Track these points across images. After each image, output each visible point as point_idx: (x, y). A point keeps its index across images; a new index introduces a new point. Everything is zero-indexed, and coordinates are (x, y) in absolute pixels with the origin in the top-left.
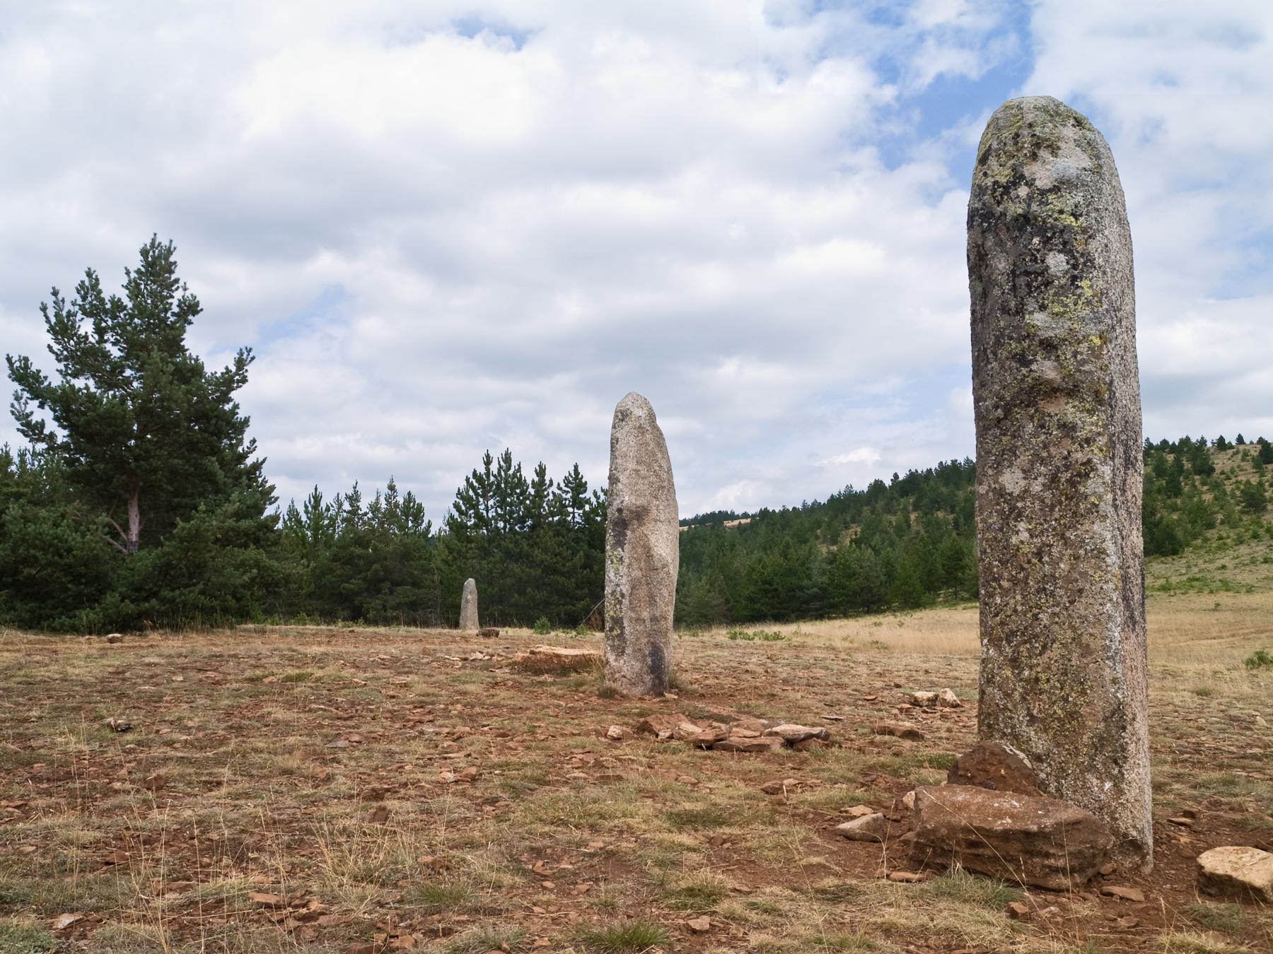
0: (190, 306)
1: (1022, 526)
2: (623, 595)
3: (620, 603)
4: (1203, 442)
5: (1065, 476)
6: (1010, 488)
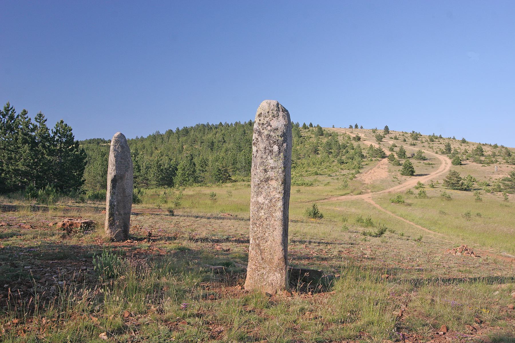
0: (170, 184)
1: (262, 211)
2: (114, 206)
3: (113, 208)
4: (232, 124)
5: (274, 200)
6: (260, 201)
